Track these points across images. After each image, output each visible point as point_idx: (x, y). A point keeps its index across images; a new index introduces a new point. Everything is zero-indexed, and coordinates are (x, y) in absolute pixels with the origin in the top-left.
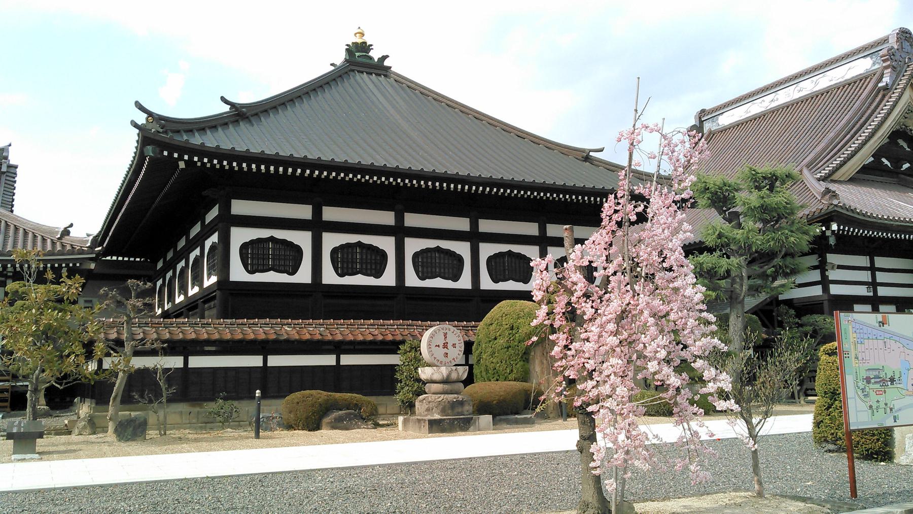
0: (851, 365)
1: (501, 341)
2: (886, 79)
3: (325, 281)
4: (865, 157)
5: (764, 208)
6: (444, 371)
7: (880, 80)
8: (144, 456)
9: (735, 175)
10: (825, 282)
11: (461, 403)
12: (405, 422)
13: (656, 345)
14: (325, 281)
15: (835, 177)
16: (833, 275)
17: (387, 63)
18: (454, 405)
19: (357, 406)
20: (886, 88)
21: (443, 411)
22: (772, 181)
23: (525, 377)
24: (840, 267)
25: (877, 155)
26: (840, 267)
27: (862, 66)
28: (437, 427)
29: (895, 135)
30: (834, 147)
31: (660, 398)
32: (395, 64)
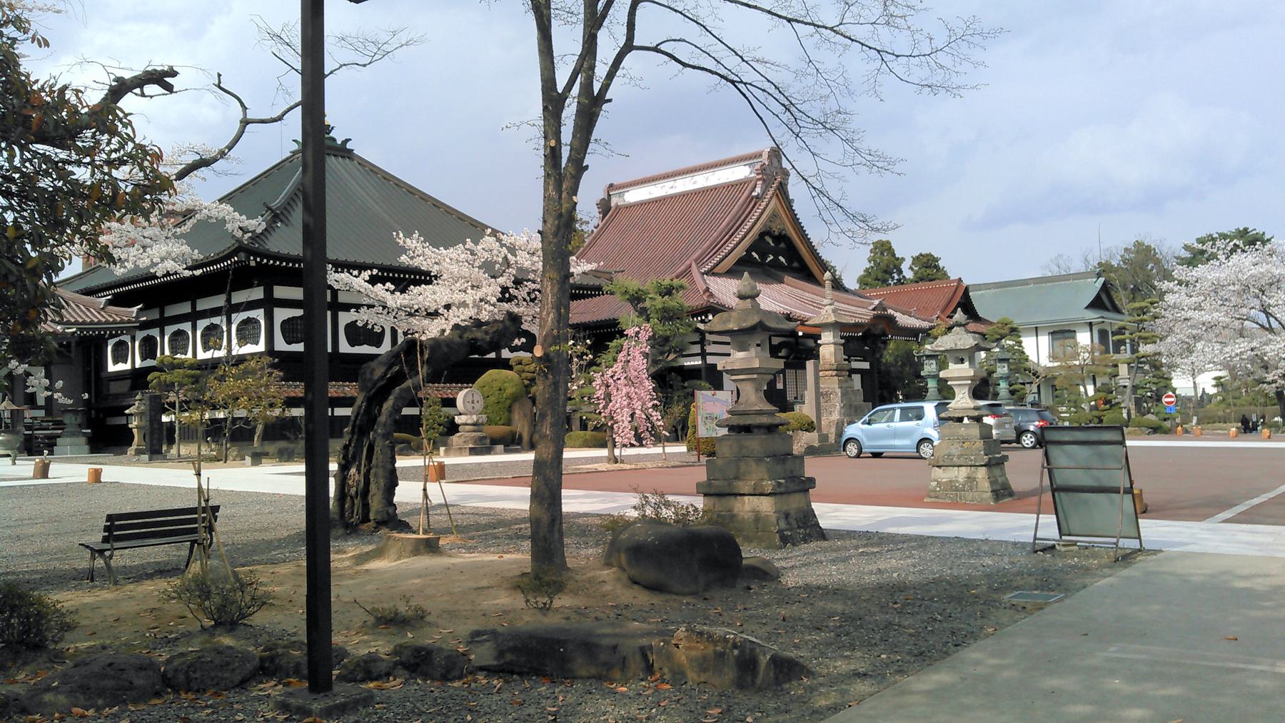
0: (701, 412)
1: (492, 399)
2: (758, 190)
3: (341, 351)
4: (740, 252)
5: (665, 310)
6: (475, 418)
7: (753, 189)
8: (221, 488)
9: (649, 285)
10: (703, 354)
11: (484, 438)
12: (446, 451)
13: (638, 405)
14: (341, 351)
15: (715, 271)
16: (709, 349)
17: (349, 146)
18: (482, 438)
19: (408, 442)
20: (757, 197)
21: (475, 443)
22: (669, 291)
23: (509, 423)
24: (714, 343)
25: (749, 251)
26: (714, 343)
27: (741, 172)
28: (473, 451)
29: (762, 235)
30: (716, 247)
31: (182, 654)
32: (360, 148)
